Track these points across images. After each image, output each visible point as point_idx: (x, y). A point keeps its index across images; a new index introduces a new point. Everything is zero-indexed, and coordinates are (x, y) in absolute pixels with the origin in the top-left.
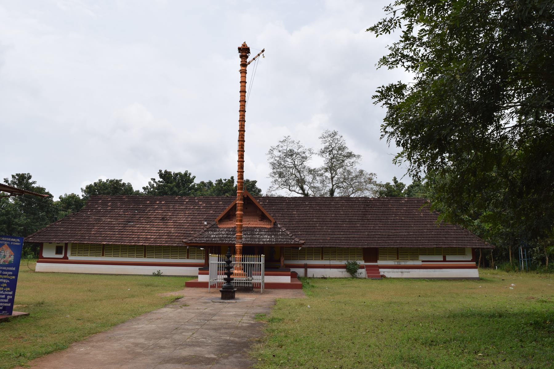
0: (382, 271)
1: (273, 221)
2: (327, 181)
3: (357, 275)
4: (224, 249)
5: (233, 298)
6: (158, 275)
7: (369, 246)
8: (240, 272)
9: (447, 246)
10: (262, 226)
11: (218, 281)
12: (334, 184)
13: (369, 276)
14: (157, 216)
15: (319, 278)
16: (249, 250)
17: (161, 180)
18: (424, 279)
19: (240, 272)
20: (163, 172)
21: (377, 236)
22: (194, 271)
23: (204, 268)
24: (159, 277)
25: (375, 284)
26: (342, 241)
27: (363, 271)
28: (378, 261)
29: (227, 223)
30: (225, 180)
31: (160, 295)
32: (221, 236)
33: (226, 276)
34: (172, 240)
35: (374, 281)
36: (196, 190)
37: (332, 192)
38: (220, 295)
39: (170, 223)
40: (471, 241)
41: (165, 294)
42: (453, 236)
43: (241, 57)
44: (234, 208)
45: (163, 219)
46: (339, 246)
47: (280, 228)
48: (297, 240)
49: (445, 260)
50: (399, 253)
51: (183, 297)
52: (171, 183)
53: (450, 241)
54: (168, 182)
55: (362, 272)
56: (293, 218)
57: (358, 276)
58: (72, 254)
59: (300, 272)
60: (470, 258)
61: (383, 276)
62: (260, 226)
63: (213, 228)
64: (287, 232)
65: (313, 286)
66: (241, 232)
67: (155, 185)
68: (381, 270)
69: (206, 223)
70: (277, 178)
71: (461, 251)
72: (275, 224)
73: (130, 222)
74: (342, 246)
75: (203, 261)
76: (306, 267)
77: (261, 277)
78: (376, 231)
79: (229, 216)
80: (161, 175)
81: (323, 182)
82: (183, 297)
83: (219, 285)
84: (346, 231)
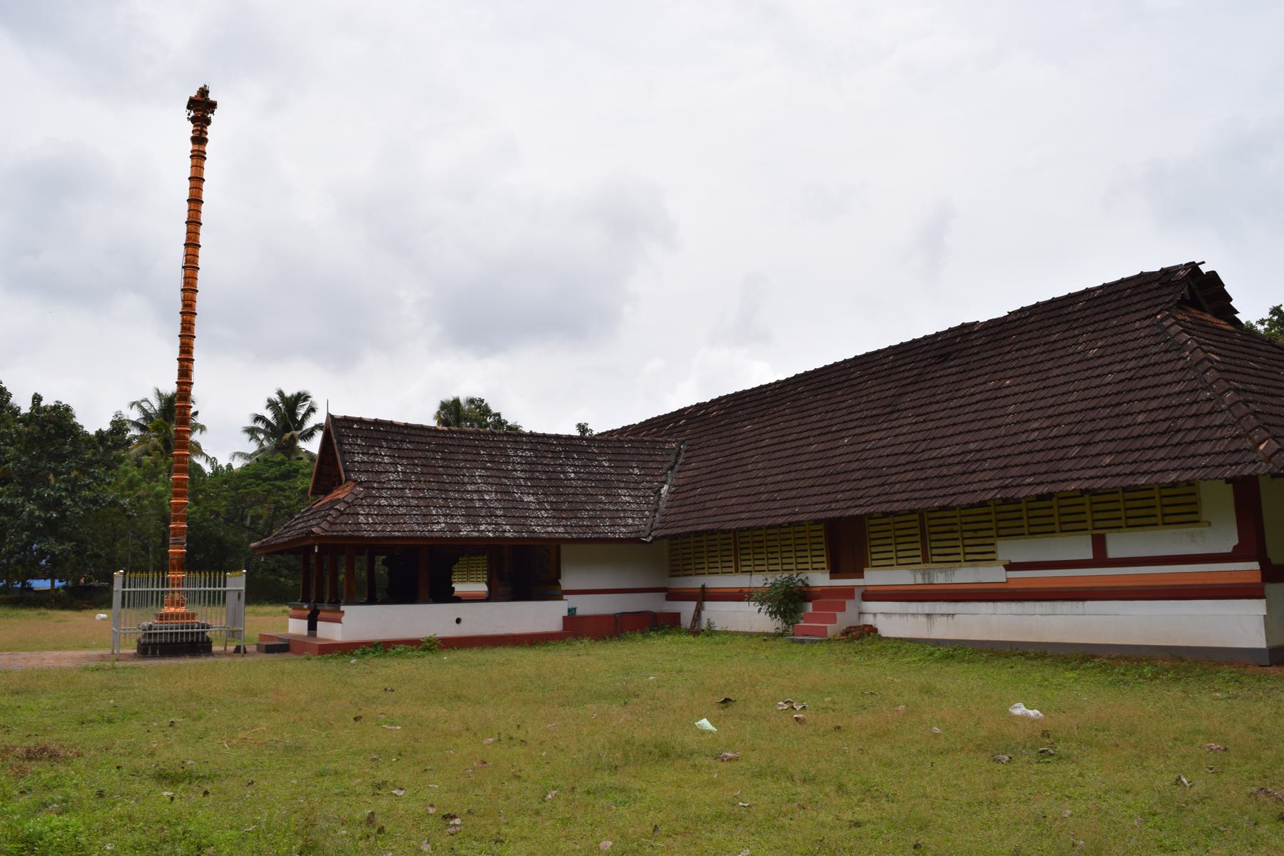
25: (816, 669)
35: (496, 650)
43: (193, 120)
49: (1100, 559)
60: (1227, 540)
61: (863, 634)
71: (1179, 507)
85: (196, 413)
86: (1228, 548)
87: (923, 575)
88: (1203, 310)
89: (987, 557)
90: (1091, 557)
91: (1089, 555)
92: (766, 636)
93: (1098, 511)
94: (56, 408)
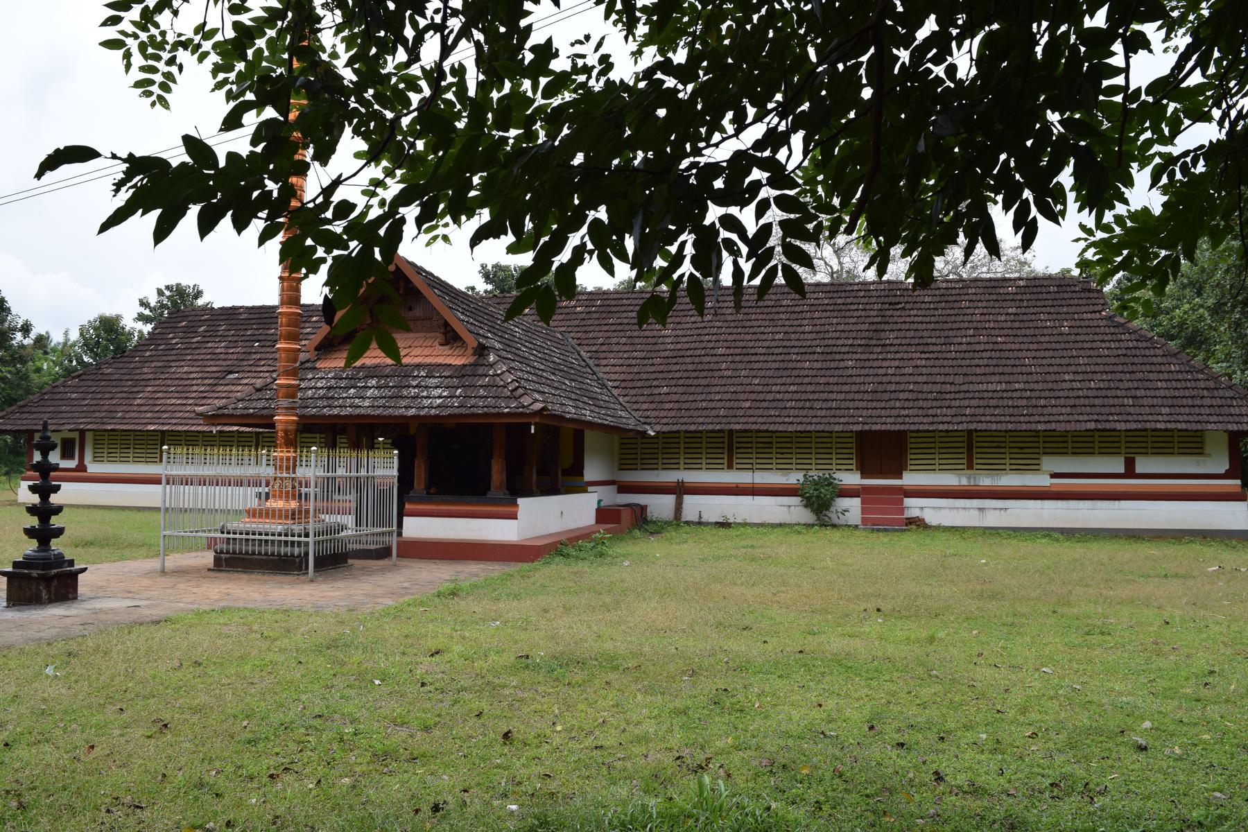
0: (914, 507)
1: (472, 342)
3: (834, 516)
7: (867, 428)
9: (1134, 426)
13: (864, 521)
17: (490, 287)
18: (1047, 533)
20: (489, 267)
21: (902, 396)
26: (786, 412)
27: (854, 505)
40: (1225, 410)
42: (1162, 393)
47: (491, 365)
49: (1130, 473)
50: (972, 447)
53: (1148, 410)
55: (852, 508)
56: (657, 347)
57: (835, 520)
58: (96, 459)
60: (1223, 467)
61: (917, 523)
68: (909, 502)
71: (1192, 443)
73: (231, 372)
74: (781, 428)
76: (680, 490)
78: (903, 379)
80: (487, 277)
84: (806, 380)
86: (1222, 471)
87: (969, 478)
89: (1035, 468)
90: (1123, 471)
91: (1121, 469)
92: (809, 526)
93: (1132, 443)
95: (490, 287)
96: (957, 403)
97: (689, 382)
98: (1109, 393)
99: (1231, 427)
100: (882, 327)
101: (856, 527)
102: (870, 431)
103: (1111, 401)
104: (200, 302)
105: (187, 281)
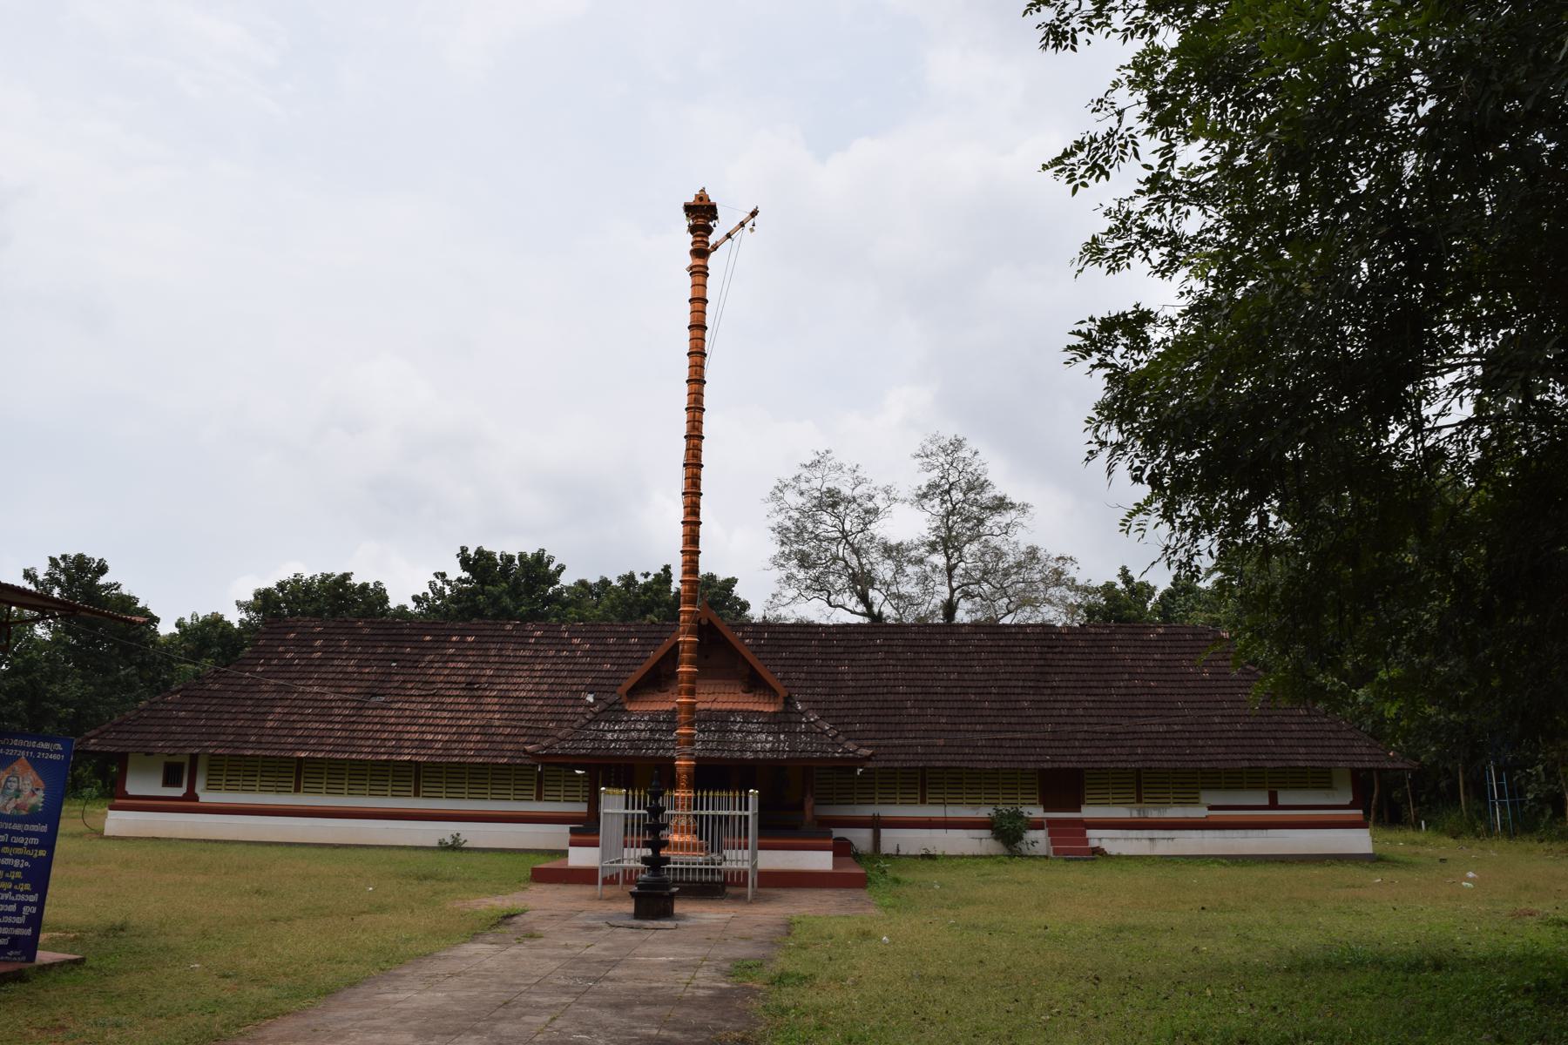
0: (1095, 837)
1: (783, 693)
2: (938, 578)
3: (1024, 848)
4: (645, 775)
5: (667, 913)
6: (455, 847)
7: (1056, 765)
8: (688, 838)
10: (751, 707)
11: (626, 864)
12: (955, 585)
13: (1056, 852)
14: (454, 679)
15: (916, 857)
16: (714, 775)
17: (466, 575)
19: (688, 838)
22: (556, 835)
23: (586, 829)
24: (457, 854)
25: (1075, 874)
28: (1084, 808)
29: (651, 698)
30: (646, 575)
31: (458, 904)
32: (634, 734)
33: (648, 852)
34: (494, 746)
36: (566, 604)
37: (950, 608)
38: (630, 907)
39: (491, 699)
40: (1348, 750)
41: (473, 902)
43: (692, 229)
44: (672, 656)
45: (469, 686)
46: (971, 765)
47: (802, 713)
48: (851, 746)
49: (1273, 805)
51: (523, 912)
52: (494, 583)
53: (1288, 750)
54: (483, 582)
55: (1038, 840)
58: (210, 787)
59: (861, 838)
60: (1348, 800)
61: (1098, 852)
62: (745, 707)
63: (612, 712)
64: (821, 723)
65: (897, 881)
66: (691, 724)
67: (448, 591)
68: (1090, 833)
69: (590, 698)
70: (795, 571)
71: (1320, 779)
72: (788, 701)
73: (375, 695)
74: (979, 765)
75: (581, 808)
76: (877, 824)
77: (747, 854)
79: (659, 678)
80: (465, 562)
81: (924, 579)
82: (523, 912)
83: (629, 876)
85: (28, 575)
88: (1465, 773)
89: (1195, 802)
94: (130, 598)
95: (466, 575)
96: (1129, 743)
97: (881, 719)
98: (1253, 735)
99: (1356, 765)
100: (1047, 669)
101: (1046, 857)
102: (1059, 769)
103: (1257, 742)
104: (103, 580)
105: (94, 553)
